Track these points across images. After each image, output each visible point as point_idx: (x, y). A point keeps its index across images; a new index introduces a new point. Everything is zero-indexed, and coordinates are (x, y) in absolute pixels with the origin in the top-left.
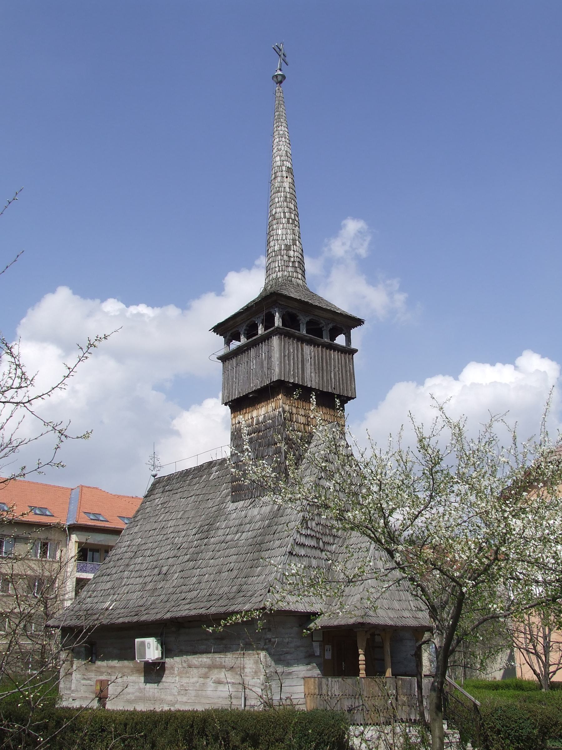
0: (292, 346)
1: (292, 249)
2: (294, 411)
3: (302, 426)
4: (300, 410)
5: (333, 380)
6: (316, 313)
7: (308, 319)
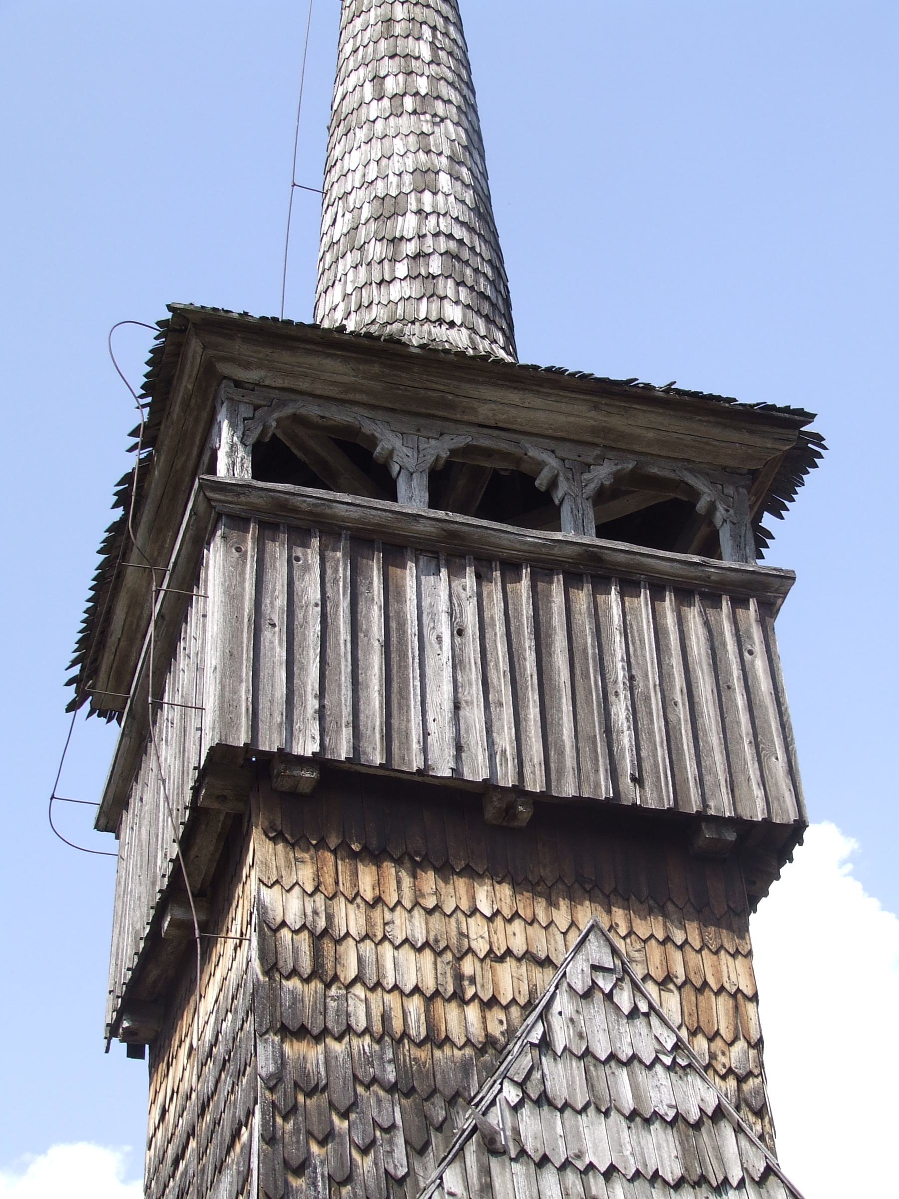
0: (311, 575)
1: (413, 205)
2: (349, 919)
3: (415, 1005)
4: (399, 916)
5: (626, 740)
6: (484, 412)
7: (438, 448)
